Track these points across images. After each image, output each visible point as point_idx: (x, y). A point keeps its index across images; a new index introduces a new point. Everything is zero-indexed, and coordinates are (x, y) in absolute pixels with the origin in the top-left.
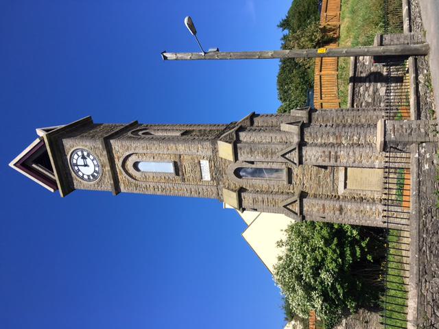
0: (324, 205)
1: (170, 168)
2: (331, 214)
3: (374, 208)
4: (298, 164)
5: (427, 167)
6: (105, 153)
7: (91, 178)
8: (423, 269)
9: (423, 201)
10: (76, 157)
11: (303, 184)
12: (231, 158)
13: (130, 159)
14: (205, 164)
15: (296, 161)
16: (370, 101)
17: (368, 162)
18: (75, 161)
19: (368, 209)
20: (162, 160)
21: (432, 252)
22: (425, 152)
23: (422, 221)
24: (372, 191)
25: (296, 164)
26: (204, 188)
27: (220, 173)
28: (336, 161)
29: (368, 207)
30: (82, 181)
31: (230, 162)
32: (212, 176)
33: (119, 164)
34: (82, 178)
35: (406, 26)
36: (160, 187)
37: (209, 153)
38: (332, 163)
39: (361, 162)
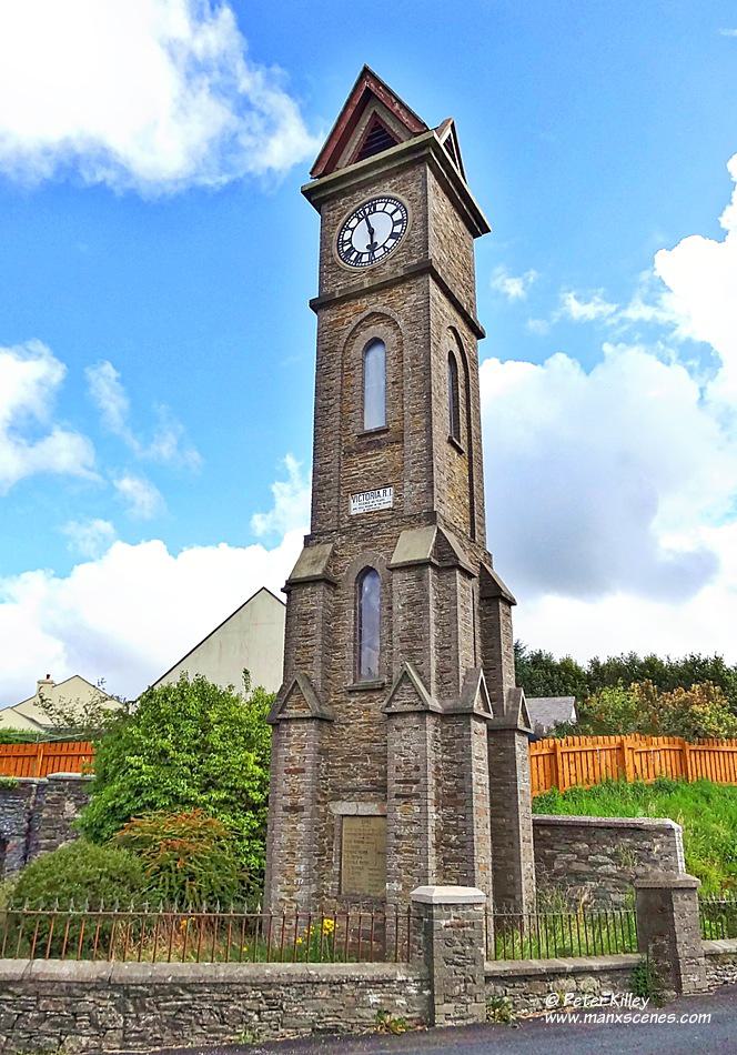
0: (303, 771)
1: (373, 419)
2: (285, 787)
3: (301, 880)
4: (388, 710)
5: (373, 998)
6: (401, 272)
7: (346, 248)
8: (141, 992)
9: (294, 991)
10: (390, 208)
11: (347, 725)
12: (398, 558)
13: (390, 330)
14: (386, 500)
15: (395, 707)
16: (557, 865)
17: (399, 866)
18: (379, 207)
19: (297, 868)
20: (390, 403)
21: (180, 1011)
22: (407, 995)
23: (249, 988)
24: (340, 875)
25: (388, 705)
26: (334, 502)
27: (365, 535)
28: (397, 796)
29: (302, 868)
30: (338, 228)
31: (390, 559)
32: (359, 517)
33: (377, 304)
34: (345, 228)
35: (258, 932)
36: (330, 402)
37: (409, 508)
38: (394, 787)
39: (397, 852)
